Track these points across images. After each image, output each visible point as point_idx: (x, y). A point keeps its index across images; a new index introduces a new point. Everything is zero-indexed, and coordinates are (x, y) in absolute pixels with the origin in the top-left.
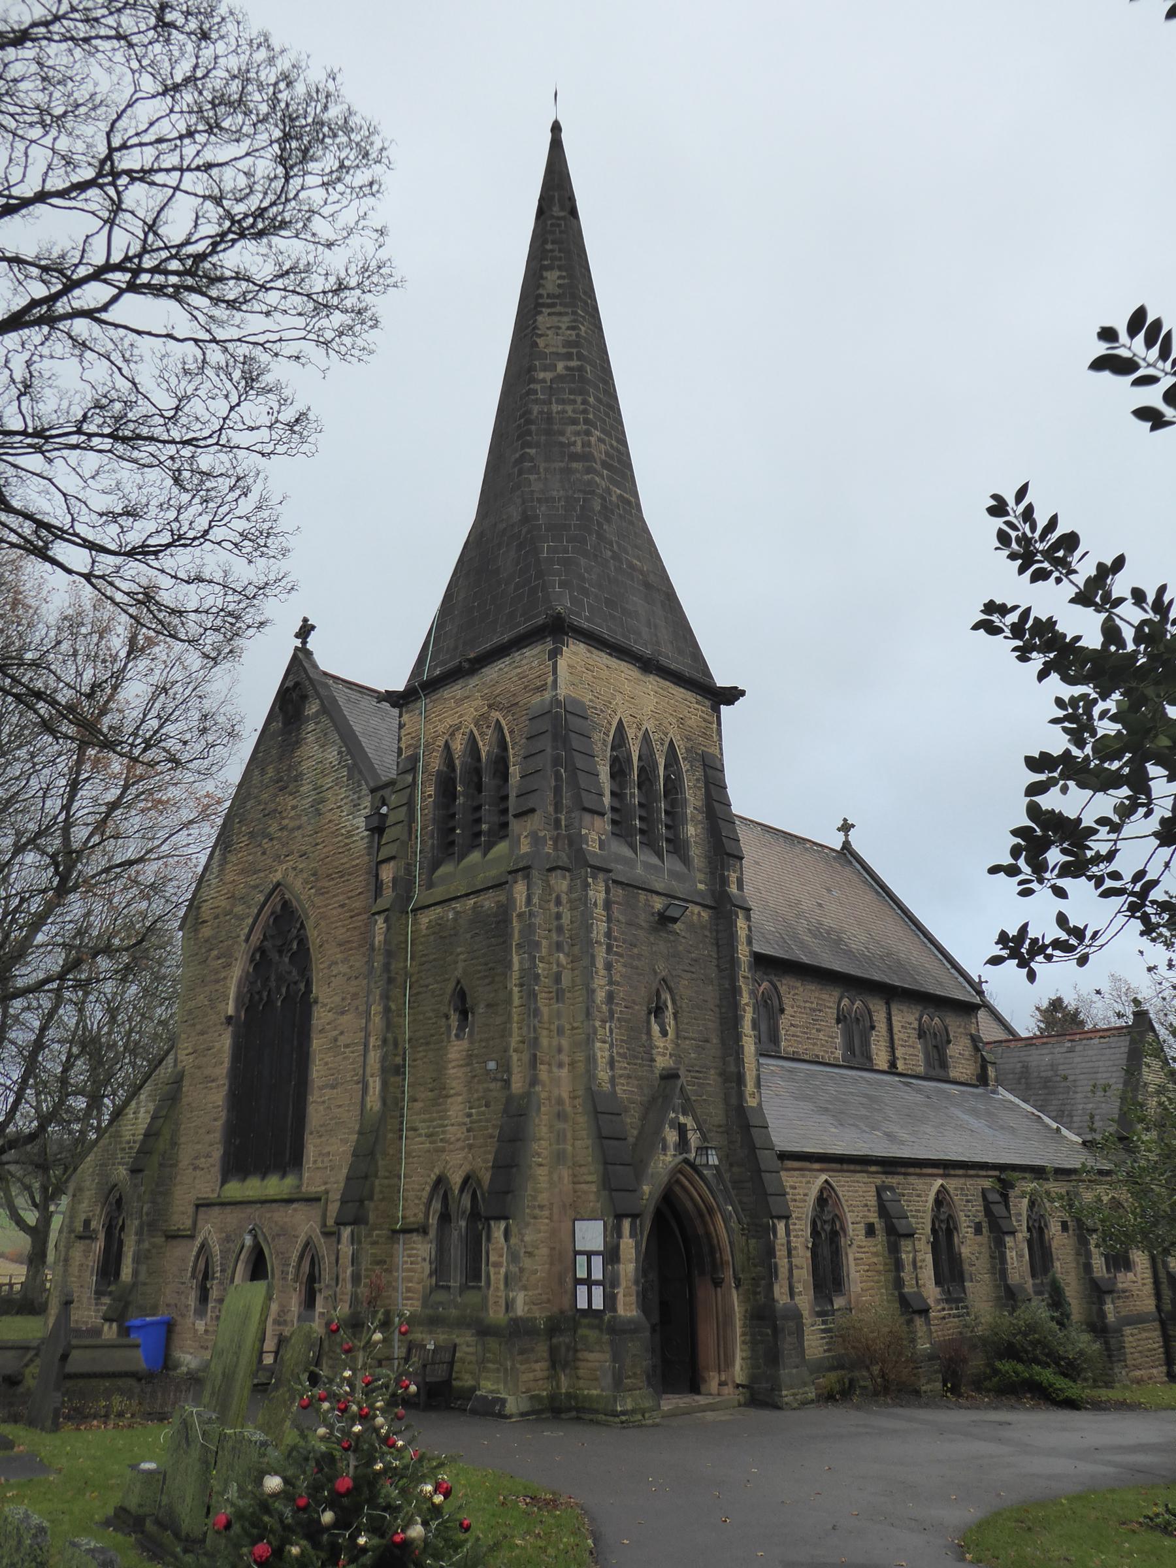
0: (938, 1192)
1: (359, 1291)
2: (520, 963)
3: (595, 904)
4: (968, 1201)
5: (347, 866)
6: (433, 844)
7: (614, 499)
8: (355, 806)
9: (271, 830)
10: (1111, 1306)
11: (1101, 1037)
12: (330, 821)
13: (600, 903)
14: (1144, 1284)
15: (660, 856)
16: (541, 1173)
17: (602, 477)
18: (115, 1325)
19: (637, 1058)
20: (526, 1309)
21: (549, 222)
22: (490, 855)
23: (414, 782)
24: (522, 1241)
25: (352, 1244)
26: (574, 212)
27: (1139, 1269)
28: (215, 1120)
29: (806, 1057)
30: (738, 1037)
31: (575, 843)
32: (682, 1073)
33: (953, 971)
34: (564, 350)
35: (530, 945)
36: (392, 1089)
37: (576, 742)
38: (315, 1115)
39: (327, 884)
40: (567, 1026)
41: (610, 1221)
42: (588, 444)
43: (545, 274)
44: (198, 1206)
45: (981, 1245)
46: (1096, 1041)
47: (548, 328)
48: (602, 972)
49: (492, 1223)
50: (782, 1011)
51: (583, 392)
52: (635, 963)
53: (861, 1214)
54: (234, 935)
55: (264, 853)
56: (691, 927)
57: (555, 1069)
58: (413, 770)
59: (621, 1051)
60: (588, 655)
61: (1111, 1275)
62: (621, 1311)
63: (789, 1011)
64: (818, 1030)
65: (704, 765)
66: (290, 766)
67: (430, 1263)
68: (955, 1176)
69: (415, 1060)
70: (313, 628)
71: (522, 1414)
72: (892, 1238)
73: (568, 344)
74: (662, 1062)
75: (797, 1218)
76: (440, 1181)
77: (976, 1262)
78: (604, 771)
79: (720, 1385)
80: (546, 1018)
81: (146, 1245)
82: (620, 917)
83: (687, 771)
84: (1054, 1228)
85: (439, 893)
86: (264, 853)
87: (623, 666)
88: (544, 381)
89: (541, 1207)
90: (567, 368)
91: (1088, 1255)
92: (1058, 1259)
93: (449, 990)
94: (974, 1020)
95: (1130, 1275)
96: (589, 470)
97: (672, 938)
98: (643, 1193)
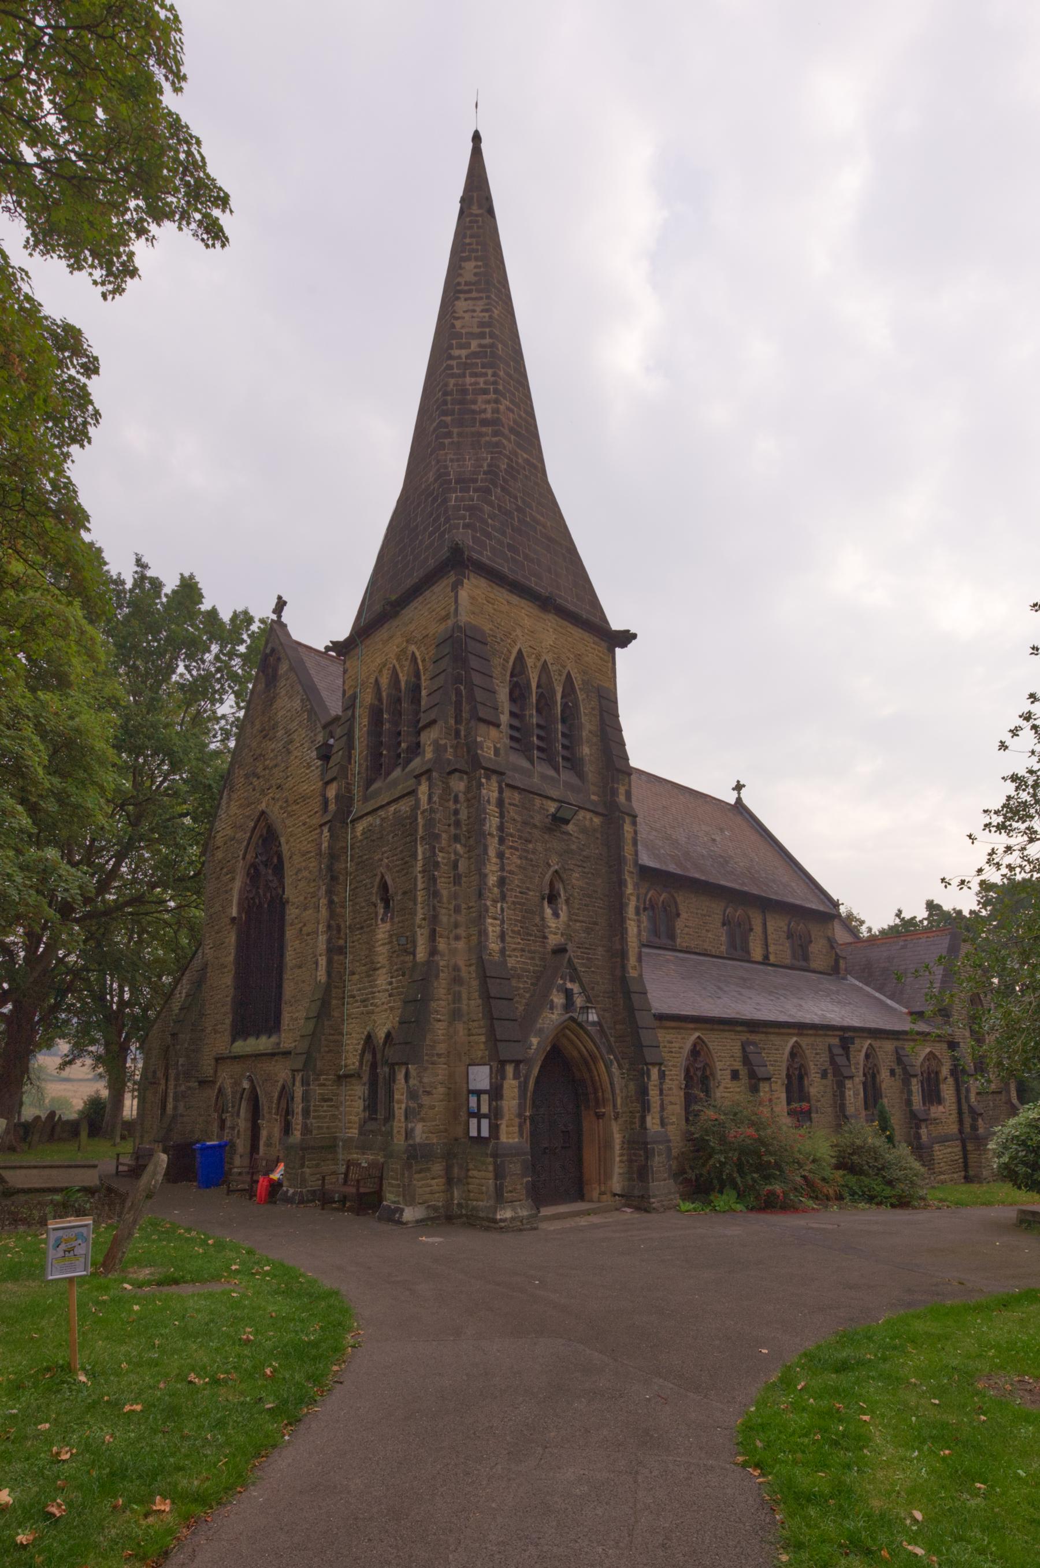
0: (793, 1047)
1: (308, 1122)
2: (423, 853)
3: (488, 801)
4: (817, 1054)
5: (308, 791)
6: (367, 766)
7: (520, 461)
8: (312, 742)
9: (259, 770)
10: (925, 1130)
11: (928, 937)
12: (296, 757)
13: (493, 801)
14: (950, 1114)
15: (556, 769)
16: (440, 1029)
17: (509, 441)
18: (160, 1144)
19: (531, 935)
20: (424, 1136)
21: (468, 219)
22: (407, 770)
23: (353, 715)
24: (421, 1082)
25: (303, 1086)
26: (491, 211)
27: (947, 1104)
28: (227, 996)
29: (697, 951)
30: (622, 920)
31: (471, 750)
32: (570, 947)
33: (816, 891)
34: (479, 330)
35: (432, 837)
36: (335, 965)
37: (474, 662)
38: (289, 990)
39: (294, 808)
40: (464, 906)
41: (494, 1064)
42: (496, 411)
43: (463, 264)
44: (217, 1060)
45: (826, 1086)
46: (924, 940)
47: (465, 312)
48: (494, 860)
49: (396, 1067)
50: (678, 915)
51: (491, 365)
52: (530, 856)
53: (728, 1063)
54: (236, 855)
55: (254, 790)
56: (584, 830)
57: (452, 942)
58: (353, 706)
59: (516, 929)
60: (490, 589)
61: (926, 1108)
62: (504, 1138)
63: (684, 915)
64: (707, 931)
65: (600, 696)
66: (270, 717)
67: (364, 1101)
68: (807, 1035)
69: (353, 942)
70: (285, 603)
71: (417, 1221)
72: (753, 1081)
73: (482, 324)
74: (553, 940)
75: (673, 1066)
76: (369, 1037)
77: (822, 1099)
78: (503, 694)
79: (600, 1194)
80: (445, 900)
81: (183, 1088)
82: (516, 817)
83: (583, 700)
84: (884, 1074)
85: (371, 806)
86: (254, 790)
87: (523, 603)
88: (459, 357)
89: (439, 1055)
90: (480, 346)
91: (910, 1092)
92: (886, 1097)
93: (376, 884)
94: (830, 927)
95: (941, 1108)
96: (496, 434)
97: (565, 837)
98: (531, 1044)
